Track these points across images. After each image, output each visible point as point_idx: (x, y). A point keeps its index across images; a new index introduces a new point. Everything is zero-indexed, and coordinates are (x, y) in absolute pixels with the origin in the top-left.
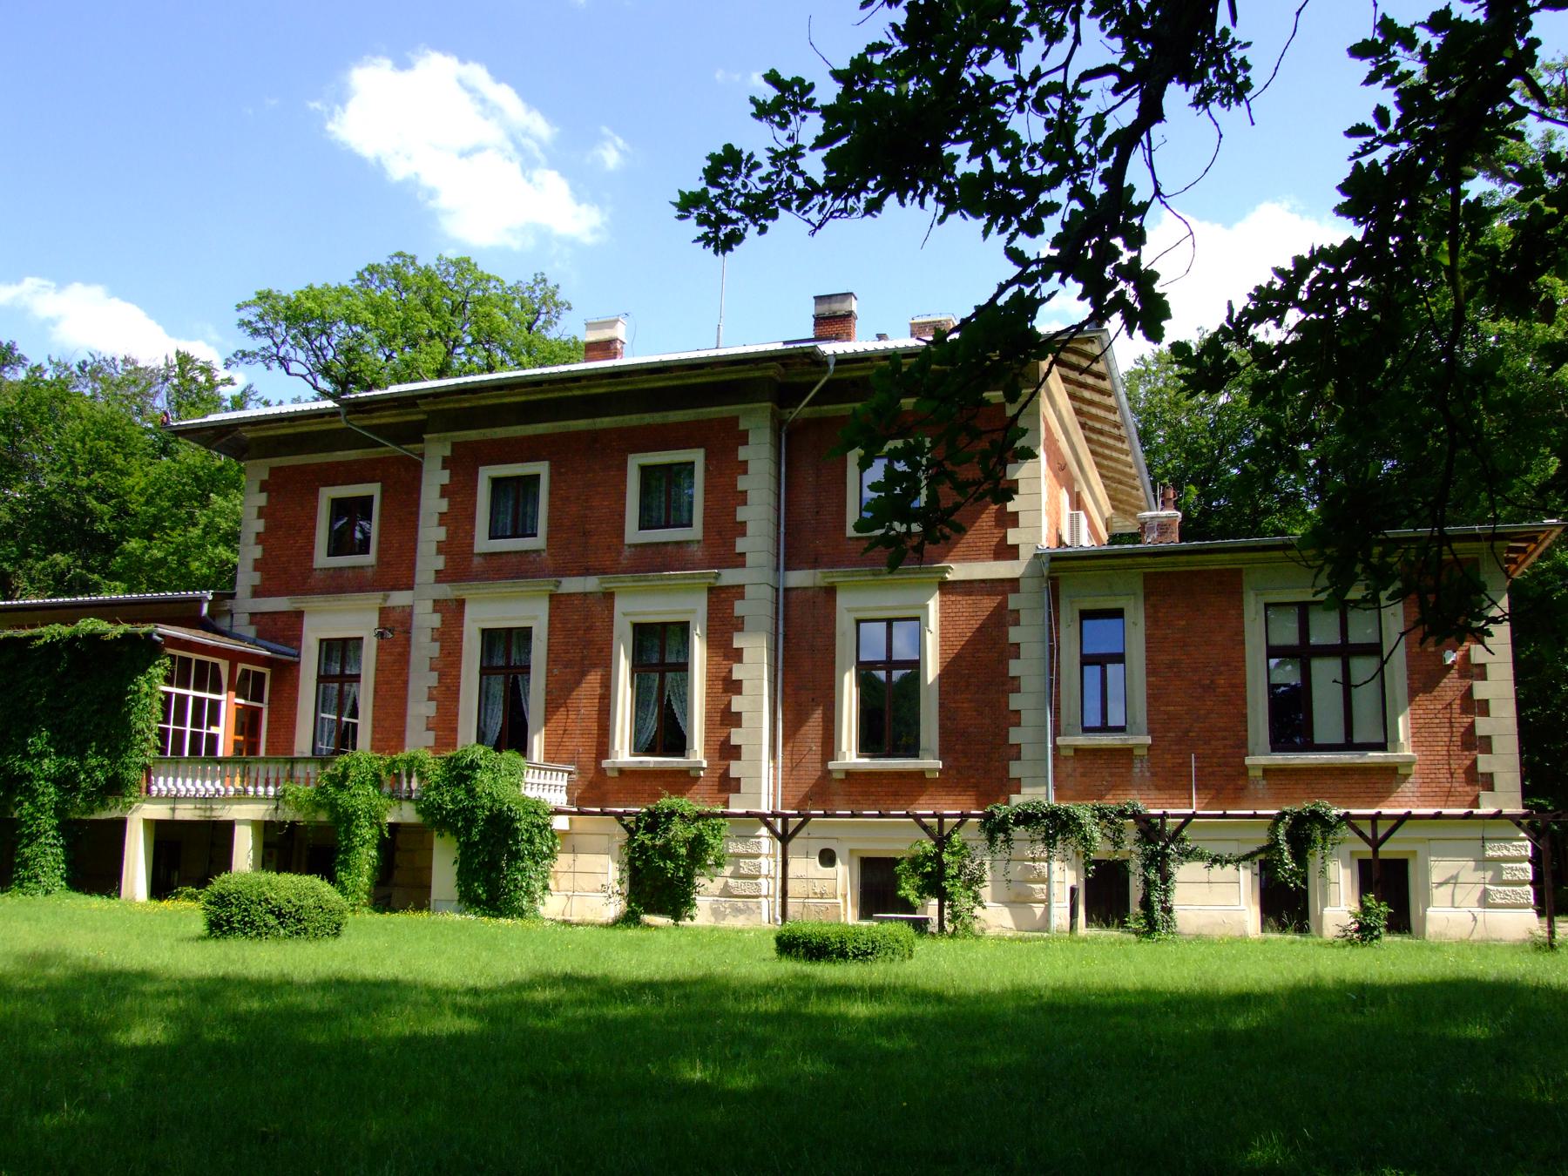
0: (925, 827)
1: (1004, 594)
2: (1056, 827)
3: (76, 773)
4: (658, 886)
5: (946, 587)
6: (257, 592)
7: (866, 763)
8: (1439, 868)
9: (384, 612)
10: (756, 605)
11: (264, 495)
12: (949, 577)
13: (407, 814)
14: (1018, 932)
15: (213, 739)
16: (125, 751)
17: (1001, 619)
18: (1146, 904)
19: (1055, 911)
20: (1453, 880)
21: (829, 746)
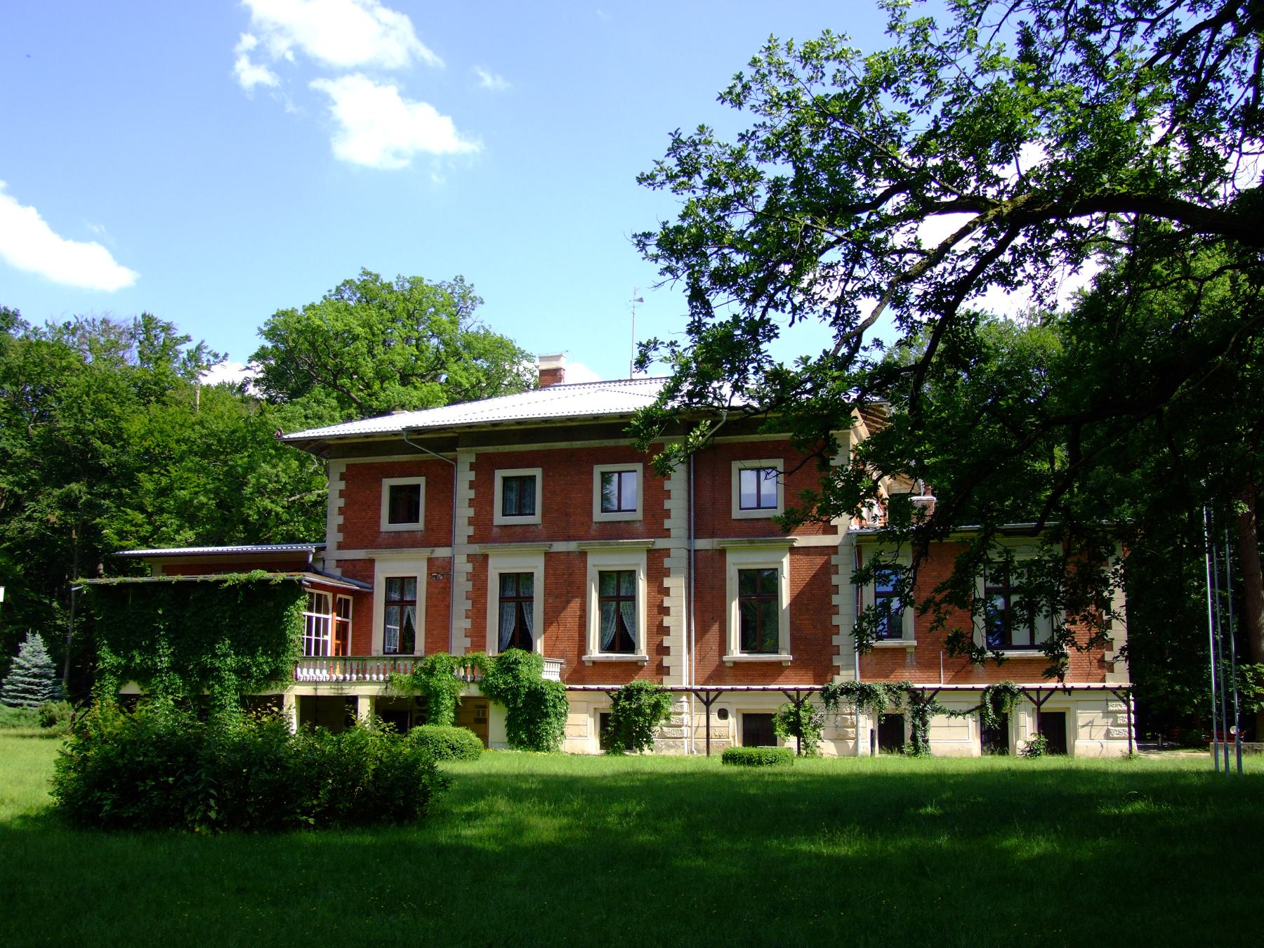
0: (789, 696)
1: (829, 555)
2: (864, 695)
3: (250, 667)
4: (622, 729)
5: (794, 551)
6: (341, 546)
7: (746, 657)
8: (1083, 717)
9: (430, 561)
10: (677, 560)
12: (795, 545)
13: (474, 691)
14: (844, 747)
15: (325, 642)
17: (827, 570)
18: (914, 738)
19: (860, 744)
20: (1090, 724)
21: (723, 646)
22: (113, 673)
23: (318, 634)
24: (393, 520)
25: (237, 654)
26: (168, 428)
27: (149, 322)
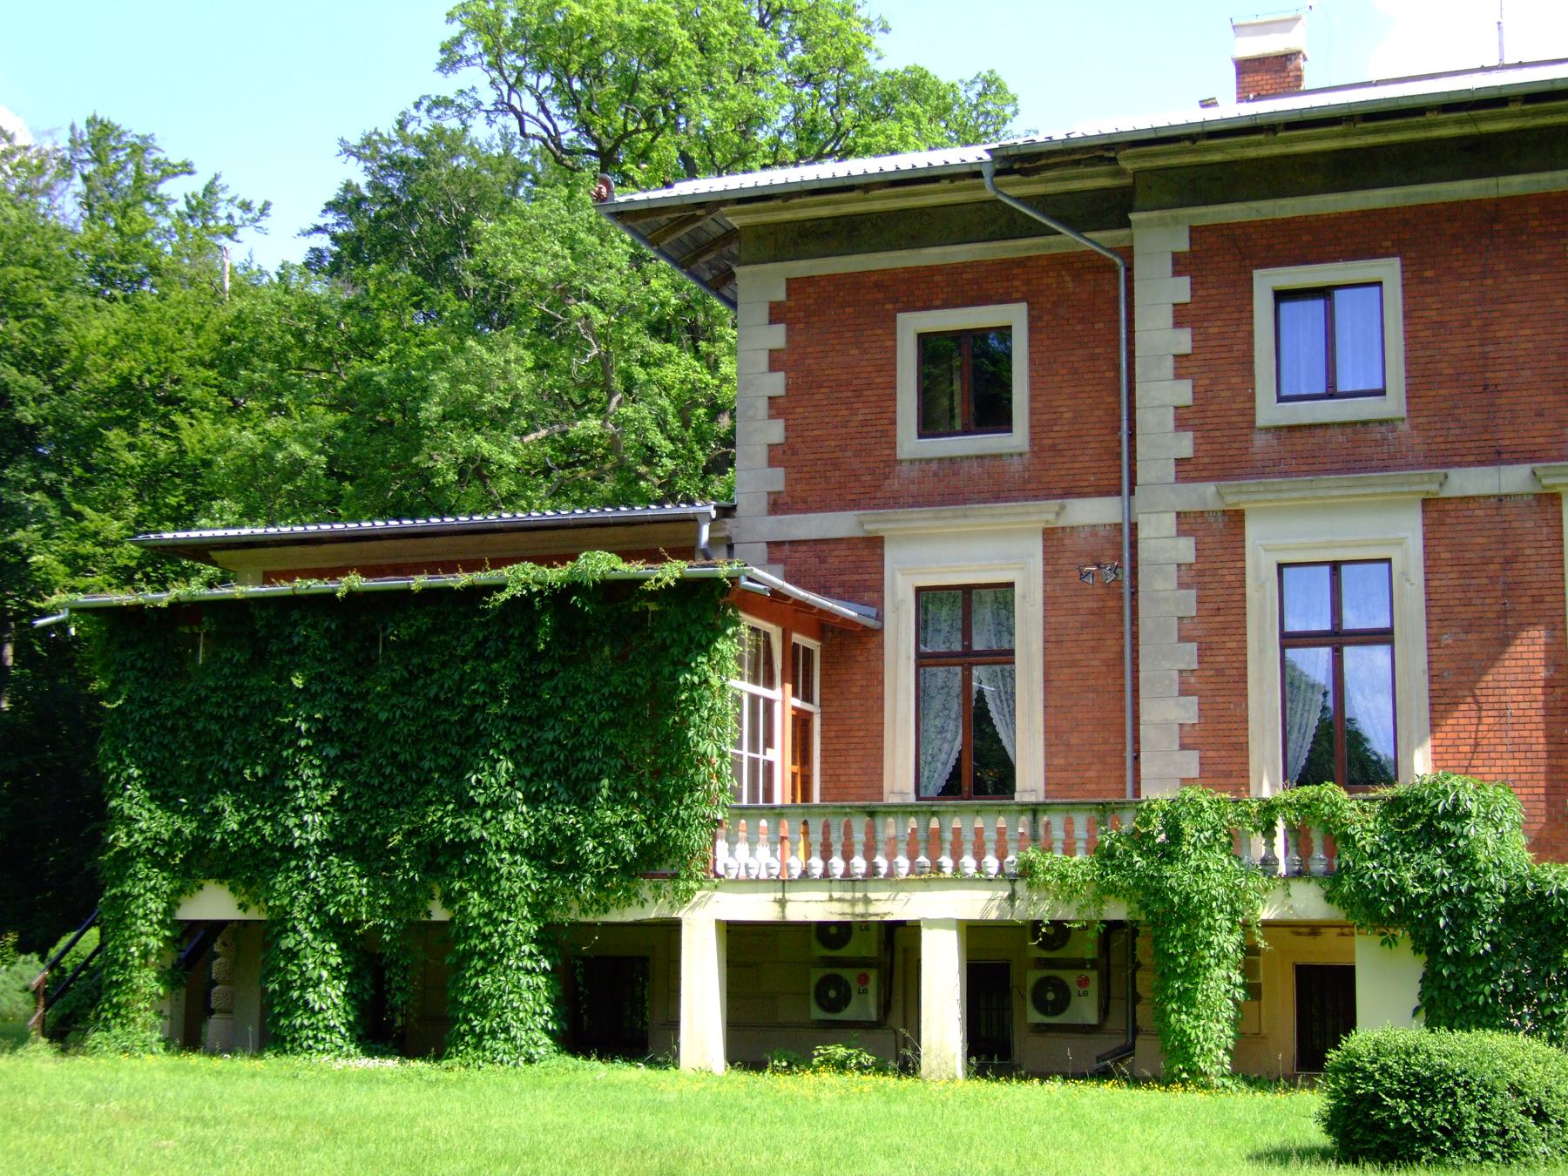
3: (573, 840)
6: (777, 505)
9: (1052, 538)
11: (781, 329)
13: (1307, 902)
15: (769, 766)
16: (679, 792)
22: (161, 863)
23: (754, 747)
24: (928, 427)
25: (532, 800)
26: (171, 332)
27: (101, 137)
